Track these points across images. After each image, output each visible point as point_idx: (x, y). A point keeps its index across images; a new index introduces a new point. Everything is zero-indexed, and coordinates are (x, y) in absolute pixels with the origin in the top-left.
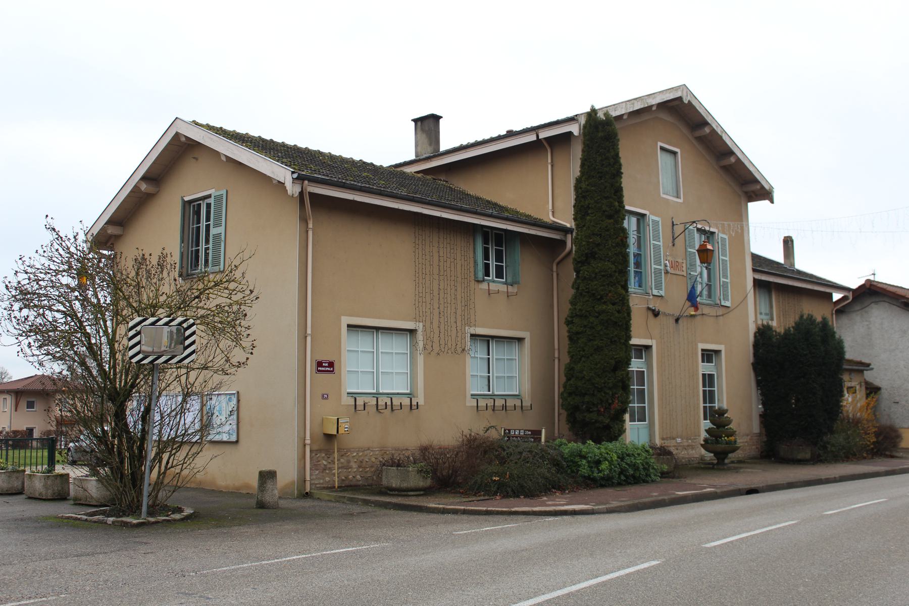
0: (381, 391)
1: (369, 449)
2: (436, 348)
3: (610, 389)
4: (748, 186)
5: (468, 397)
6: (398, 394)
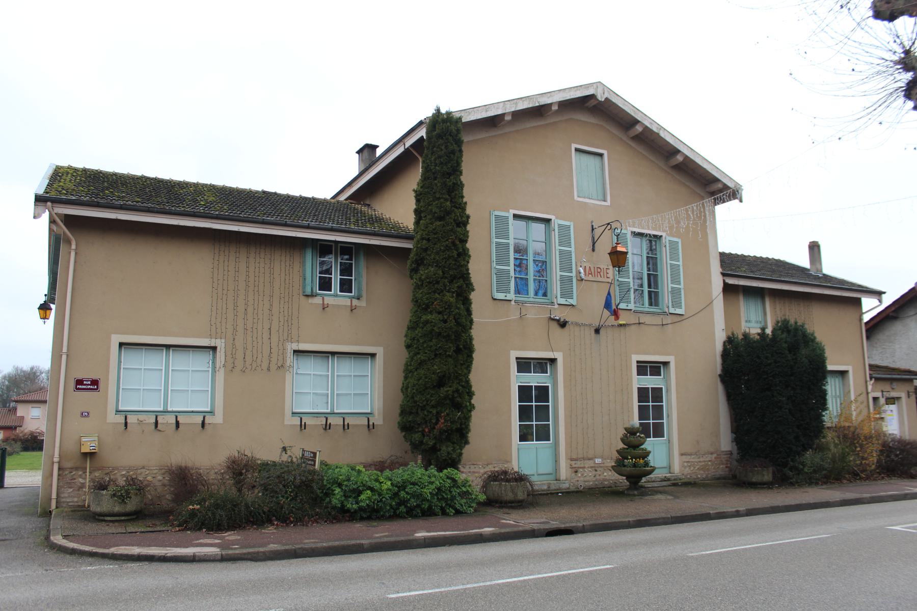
0: (169, 409)
1: (143, 468)
2: (239, 364)
3: (433, 407)
4: (710, 187)
5: (288, 413)
6: (193, 412)
